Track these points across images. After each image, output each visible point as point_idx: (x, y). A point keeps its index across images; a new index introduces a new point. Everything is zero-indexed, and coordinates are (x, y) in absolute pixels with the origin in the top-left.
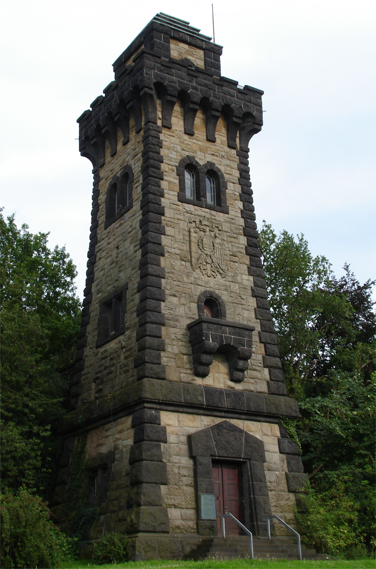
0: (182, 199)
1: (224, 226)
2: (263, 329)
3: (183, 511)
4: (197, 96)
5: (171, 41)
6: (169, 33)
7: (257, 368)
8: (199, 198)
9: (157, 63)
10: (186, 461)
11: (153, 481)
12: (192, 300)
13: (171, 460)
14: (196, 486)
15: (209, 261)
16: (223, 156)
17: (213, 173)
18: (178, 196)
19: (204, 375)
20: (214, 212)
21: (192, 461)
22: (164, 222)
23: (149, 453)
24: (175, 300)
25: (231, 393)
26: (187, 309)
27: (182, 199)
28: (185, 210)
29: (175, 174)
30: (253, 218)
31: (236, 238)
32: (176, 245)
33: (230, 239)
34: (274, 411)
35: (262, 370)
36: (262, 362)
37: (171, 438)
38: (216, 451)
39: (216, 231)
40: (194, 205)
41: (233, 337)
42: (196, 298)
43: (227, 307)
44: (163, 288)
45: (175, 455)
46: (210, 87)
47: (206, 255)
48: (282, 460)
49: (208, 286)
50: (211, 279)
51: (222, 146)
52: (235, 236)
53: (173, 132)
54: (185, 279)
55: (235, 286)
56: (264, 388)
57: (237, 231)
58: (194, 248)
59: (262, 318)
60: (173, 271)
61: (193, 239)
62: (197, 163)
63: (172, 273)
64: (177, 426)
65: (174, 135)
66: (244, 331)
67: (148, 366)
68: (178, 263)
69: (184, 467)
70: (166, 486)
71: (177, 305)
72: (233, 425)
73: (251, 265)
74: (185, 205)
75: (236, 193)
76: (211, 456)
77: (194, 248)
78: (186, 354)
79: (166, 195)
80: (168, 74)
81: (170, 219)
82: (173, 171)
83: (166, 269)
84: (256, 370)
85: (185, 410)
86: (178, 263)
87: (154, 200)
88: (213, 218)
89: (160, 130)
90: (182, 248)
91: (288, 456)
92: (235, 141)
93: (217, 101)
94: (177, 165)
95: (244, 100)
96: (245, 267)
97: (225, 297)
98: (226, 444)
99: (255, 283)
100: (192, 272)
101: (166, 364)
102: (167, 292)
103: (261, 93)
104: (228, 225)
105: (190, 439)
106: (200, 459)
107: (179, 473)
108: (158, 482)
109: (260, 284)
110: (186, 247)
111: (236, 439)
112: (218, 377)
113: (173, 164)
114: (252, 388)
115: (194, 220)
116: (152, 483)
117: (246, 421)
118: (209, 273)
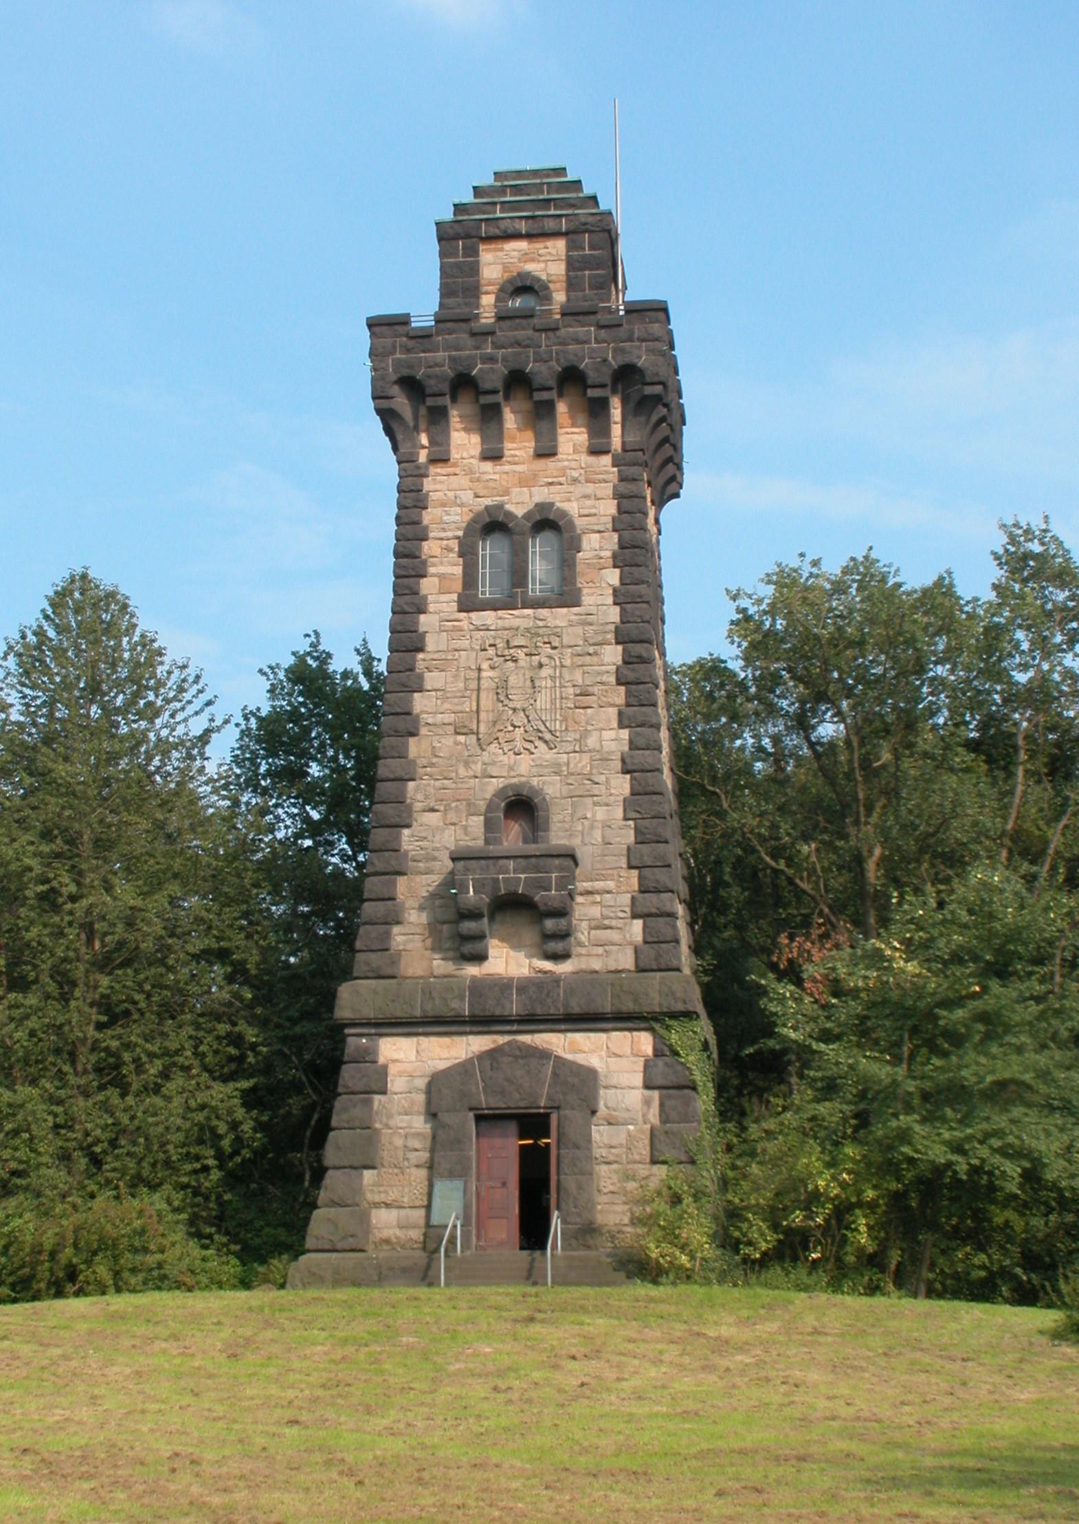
0: (468, 604)
1: (568, 634)
2: (639, 839)
3: (403, 1212)
4: (491, 374)
5: (482, 247)
6: (474, 233)
7: (614, 923)
9: (401, 336)
10: (420, 1124)
11: (346, 1163)
12: (472, 811)
13: (392, 1123)
15: (519, 719)
17: (547, 522)
18: (459, 602)
19: (481, 958)
21: (428, 1126)
22: (420, 666)
23: (345, 1116)
24: (433, 819)
25: (541, 985)
26: (460, 831)
27: (468, 604)
28: (472, 627)
29: (453, 556)
31: (596, 653)
32: (447, 706)
33: (579, 661)
34: (629, 1006)
35: (625, 924)
36: (628, 909)
37: (396, 1083)
38: (483, 1101)
40: (495, 610)
41: (522, 876)
42: (482, 805)
43: (553, 809)
44: (409, 801)
45: (400, 1114)
46: (528, 342)
47: (514, 710)
48: (647, 1102)
49: (512, 774)
50: (525, 756)
51: (576, 457)
52: (591, 651)
53: (455, 465)
54: (462, 771)
55: (580, 761)
56: (626, 960)
57: (599, 638)
58: (487, 701)
59: (638, 816)
60: (435, 760)
61: (485, 684)
62: (509, 515)
63: (432, 765)
64: (409, 1060)
65: (457, 470)
66: (549, 861)
68: (449, 741)
69: (417, 1135)
70: (375, 1172)
71: (437, 828)
72: (529, 1046)
73: (628, 705)
74: (473, 615)
75: (603, 554)
76: (471, 1109)
77: (487, 701)
78: (444, 923)
79: (431, 608)
80: (424, 352)
81: (435, 656)
82: (449, 550)
83: (418, 761)
84: (611, 928)
85: (430, 1029)
86: (447, 743)
87: (402, 624)
88: (541, 624)
89: (422, 471)
90: (459, 708)
91: (664, 1092)
94: (460, 533)
95: (614, 341)
96: (613, 712)
97: (552, 789)
98: (506, 1084)
99: (631, 742)
100: (479, 752)
101: (401, 947)
102: (418, 806)
104: (579, 630)
105: (437, 1085)
106: (444, 1117)
107: (405, 1146)
108: (356, 1164)
109: (641, 742)
111: (529, 1072)
113: (450, 534)
114: (596, 965)
115: (492, 642)
116: (345, 1167)
117: (569, 1035)
118: (519, 744)
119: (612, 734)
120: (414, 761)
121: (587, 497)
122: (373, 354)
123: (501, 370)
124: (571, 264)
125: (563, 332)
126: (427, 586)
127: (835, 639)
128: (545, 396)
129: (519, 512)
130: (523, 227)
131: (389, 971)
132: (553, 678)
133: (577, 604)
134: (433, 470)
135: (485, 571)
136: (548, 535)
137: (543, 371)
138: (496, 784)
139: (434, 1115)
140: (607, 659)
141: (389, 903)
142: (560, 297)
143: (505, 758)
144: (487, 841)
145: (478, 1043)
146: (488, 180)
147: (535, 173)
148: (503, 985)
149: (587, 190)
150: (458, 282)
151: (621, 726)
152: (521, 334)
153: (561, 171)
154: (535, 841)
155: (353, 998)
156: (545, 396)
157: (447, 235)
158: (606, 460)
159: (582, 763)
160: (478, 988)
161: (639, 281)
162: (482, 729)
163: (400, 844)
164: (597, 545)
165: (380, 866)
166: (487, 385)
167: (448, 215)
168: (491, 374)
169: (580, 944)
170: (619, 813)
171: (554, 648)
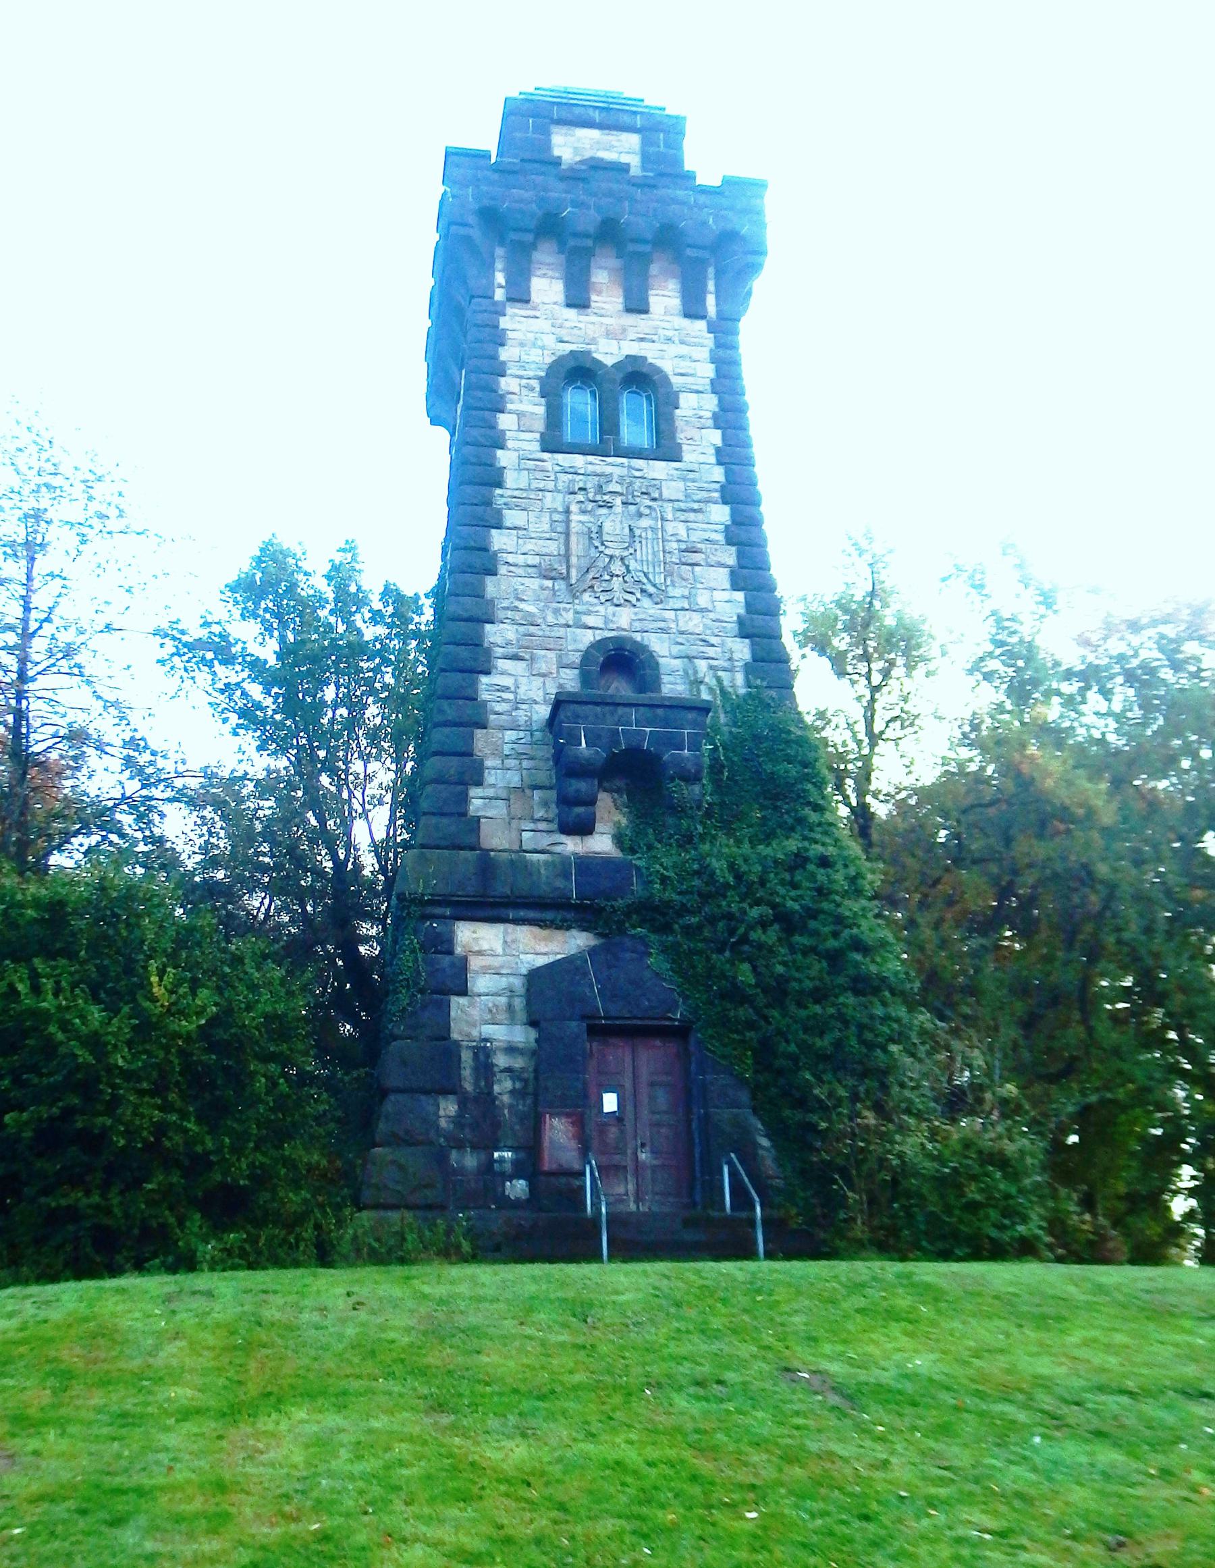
0: (552, 443)
15: (617, 568)
17: (639, 377)
27: (552, 443)
37: (481, 983)
42: (576, 658)
53: (534, 309)
65: (537, 314)
79: (510, 444)
81: (516, 493)
82: (533, 389)
89: (499, 309)
97: (659, 646)
104: (681, 485)
113: (531, 374)
119: (726, 595)
120: (492, 601)
131: (468, 840)
133: (678, 459)
134: (511, 310)
141: (466, 759)
143: (601, 609)
158: (701, 325)
159: (693, 623)
163: (476, 691)
171: (654, 499)
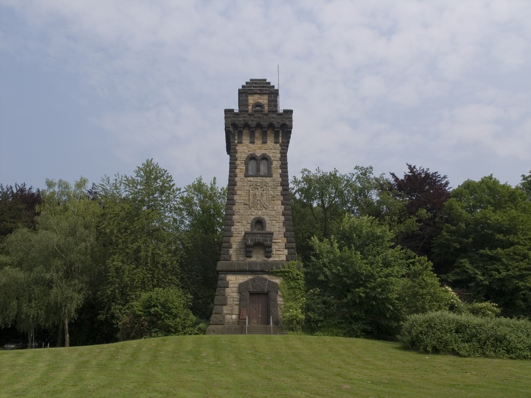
0: (246, 176)
4: (253, 124)
8: (257, 174)
10: (236, 295)
14: (240, 305)
15: (259, 202)
16: (271, 149)
17: (265, 158)
19: (251, 257)
20: (264, 178)
22: (236, 189)
25: (266, 263)
27: (246, 176)
29: (243, 164)
30: (287, 176)
37: (231, 285)
38: (252, 290)
39: (265, 187)
42: (250, 222)
50: (260, 211)
54: (246, 214)
56: (284, 258)
58: (251, 198)
62: (256, 156)
64: (234, 281)
67: (222, 256)
77: (251, 198)
82: (242, 163)
92: (279, 139)
93: (265, 123)
96: (280, 202)
97: (266, 218)
103: (291, 112)
104: (272, 183)
105: (240, 285)
106: (243, 293)
110: (247, 198)
112: (257, 258)
114: (277, 259)
118: (259, 208)
119: (280, 207)
121: (274, 153)
122: (225, 118)
123: (255, 123)
124: (269, 101)
125: (269, 116)
126: (237, 171)
127: (322, 184)
128: (265, 129)
129: (259, 155)
130: (258, 92)
132: (266, 193)
133: (272, 177)
135: (250, 168)
136: (264, 161)
137: (265, 124)
138: (253, 217)
139: (240, 293)
140: (279, 189)
142: (266, 108)
144: (252, 230)
145: (250, 277)
146: (249, 81)
147: (260, 80)
148: (256, 263)
149: (272, 84)
150: (243, 102)
151: (282, 205)
152: (259, 115)
153: (265, 80)
154: (262, 230)
155: (221, 265)
156: (265, 129)
157: (241, 92)
158: (278, 145)
159: (273, 213)
160: (250, 264)
161: (282, 106)
162: (250, 204)
164: (276, 164)
165: (227, 234)
166: (252, 126)
167: (241, 88)
168: (253, 124)
169: (273, 254)
170: (282, 224)
